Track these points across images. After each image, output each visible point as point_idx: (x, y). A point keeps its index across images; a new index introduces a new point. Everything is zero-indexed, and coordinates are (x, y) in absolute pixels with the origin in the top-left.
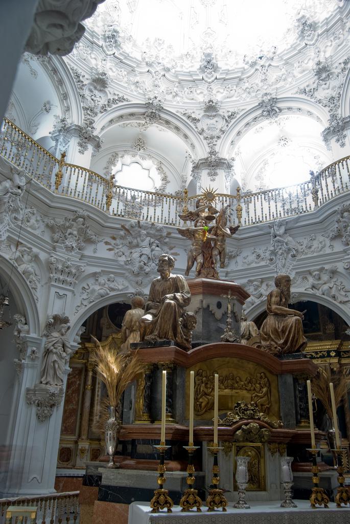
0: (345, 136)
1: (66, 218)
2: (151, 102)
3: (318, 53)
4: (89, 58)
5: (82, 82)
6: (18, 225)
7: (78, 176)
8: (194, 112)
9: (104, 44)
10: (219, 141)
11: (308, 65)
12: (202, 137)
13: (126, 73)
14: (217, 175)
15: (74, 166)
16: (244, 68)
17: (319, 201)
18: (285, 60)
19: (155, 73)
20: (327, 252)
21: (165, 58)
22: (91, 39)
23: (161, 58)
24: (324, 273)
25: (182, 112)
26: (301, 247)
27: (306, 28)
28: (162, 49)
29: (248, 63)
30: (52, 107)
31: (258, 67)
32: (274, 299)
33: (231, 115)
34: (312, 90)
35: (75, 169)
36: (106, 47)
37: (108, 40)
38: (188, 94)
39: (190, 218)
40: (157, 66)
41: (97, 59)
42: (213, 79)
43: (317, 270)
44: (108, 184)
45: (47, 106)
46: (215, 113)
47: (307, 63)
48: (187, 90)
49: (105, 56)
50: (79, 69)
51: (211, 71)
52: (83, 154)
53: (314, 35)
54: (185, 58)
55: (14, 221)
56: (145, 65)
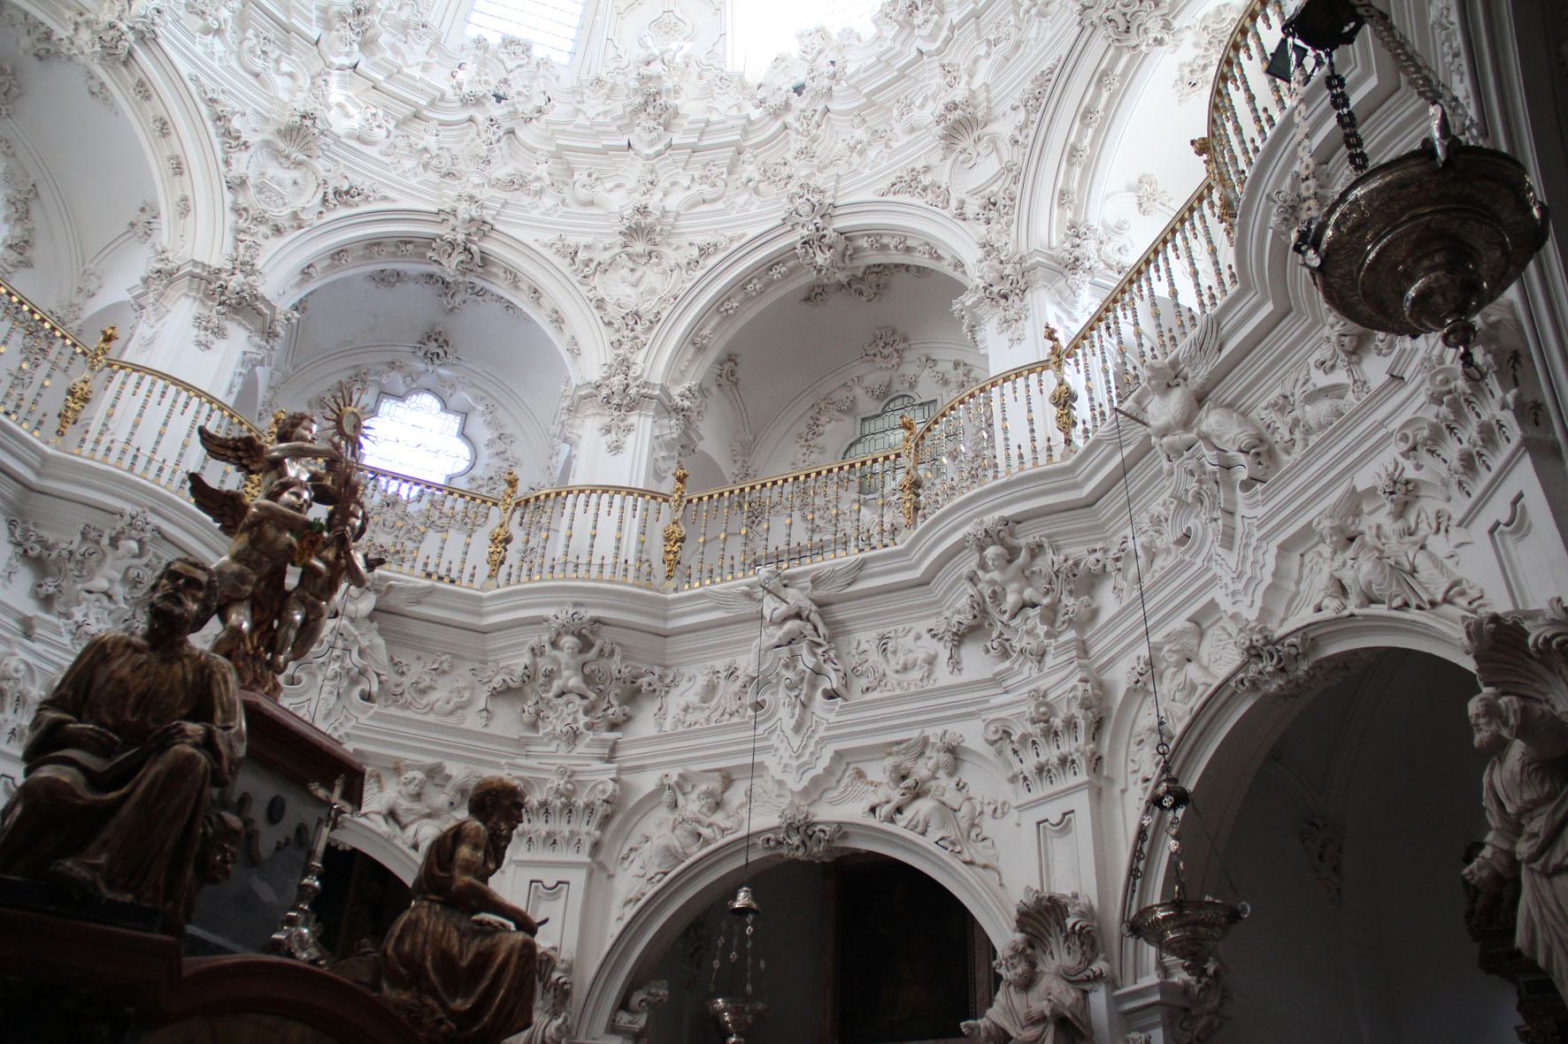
0: (629, 429)
3: (649, 186)
8: (243, 115)
10: (276, 243)
11: (611, 196)
12: (229, 197)
14: (224, 336)
16: (748, 117)
18: (558, 146)
20: (466, 725)
24: (437, 785)
26: (397, 679)
27: (650, 109)
29: (460, 86)
32: (464, 851)
33: (347, 193)
34: (593, 265)
38: (252, 51)
39: (240, 458)
42: (346, 62)
43: (420, 768)
46: (302, 157)
48: (255, 41)
51: (354, 37)
53: (659, 138)
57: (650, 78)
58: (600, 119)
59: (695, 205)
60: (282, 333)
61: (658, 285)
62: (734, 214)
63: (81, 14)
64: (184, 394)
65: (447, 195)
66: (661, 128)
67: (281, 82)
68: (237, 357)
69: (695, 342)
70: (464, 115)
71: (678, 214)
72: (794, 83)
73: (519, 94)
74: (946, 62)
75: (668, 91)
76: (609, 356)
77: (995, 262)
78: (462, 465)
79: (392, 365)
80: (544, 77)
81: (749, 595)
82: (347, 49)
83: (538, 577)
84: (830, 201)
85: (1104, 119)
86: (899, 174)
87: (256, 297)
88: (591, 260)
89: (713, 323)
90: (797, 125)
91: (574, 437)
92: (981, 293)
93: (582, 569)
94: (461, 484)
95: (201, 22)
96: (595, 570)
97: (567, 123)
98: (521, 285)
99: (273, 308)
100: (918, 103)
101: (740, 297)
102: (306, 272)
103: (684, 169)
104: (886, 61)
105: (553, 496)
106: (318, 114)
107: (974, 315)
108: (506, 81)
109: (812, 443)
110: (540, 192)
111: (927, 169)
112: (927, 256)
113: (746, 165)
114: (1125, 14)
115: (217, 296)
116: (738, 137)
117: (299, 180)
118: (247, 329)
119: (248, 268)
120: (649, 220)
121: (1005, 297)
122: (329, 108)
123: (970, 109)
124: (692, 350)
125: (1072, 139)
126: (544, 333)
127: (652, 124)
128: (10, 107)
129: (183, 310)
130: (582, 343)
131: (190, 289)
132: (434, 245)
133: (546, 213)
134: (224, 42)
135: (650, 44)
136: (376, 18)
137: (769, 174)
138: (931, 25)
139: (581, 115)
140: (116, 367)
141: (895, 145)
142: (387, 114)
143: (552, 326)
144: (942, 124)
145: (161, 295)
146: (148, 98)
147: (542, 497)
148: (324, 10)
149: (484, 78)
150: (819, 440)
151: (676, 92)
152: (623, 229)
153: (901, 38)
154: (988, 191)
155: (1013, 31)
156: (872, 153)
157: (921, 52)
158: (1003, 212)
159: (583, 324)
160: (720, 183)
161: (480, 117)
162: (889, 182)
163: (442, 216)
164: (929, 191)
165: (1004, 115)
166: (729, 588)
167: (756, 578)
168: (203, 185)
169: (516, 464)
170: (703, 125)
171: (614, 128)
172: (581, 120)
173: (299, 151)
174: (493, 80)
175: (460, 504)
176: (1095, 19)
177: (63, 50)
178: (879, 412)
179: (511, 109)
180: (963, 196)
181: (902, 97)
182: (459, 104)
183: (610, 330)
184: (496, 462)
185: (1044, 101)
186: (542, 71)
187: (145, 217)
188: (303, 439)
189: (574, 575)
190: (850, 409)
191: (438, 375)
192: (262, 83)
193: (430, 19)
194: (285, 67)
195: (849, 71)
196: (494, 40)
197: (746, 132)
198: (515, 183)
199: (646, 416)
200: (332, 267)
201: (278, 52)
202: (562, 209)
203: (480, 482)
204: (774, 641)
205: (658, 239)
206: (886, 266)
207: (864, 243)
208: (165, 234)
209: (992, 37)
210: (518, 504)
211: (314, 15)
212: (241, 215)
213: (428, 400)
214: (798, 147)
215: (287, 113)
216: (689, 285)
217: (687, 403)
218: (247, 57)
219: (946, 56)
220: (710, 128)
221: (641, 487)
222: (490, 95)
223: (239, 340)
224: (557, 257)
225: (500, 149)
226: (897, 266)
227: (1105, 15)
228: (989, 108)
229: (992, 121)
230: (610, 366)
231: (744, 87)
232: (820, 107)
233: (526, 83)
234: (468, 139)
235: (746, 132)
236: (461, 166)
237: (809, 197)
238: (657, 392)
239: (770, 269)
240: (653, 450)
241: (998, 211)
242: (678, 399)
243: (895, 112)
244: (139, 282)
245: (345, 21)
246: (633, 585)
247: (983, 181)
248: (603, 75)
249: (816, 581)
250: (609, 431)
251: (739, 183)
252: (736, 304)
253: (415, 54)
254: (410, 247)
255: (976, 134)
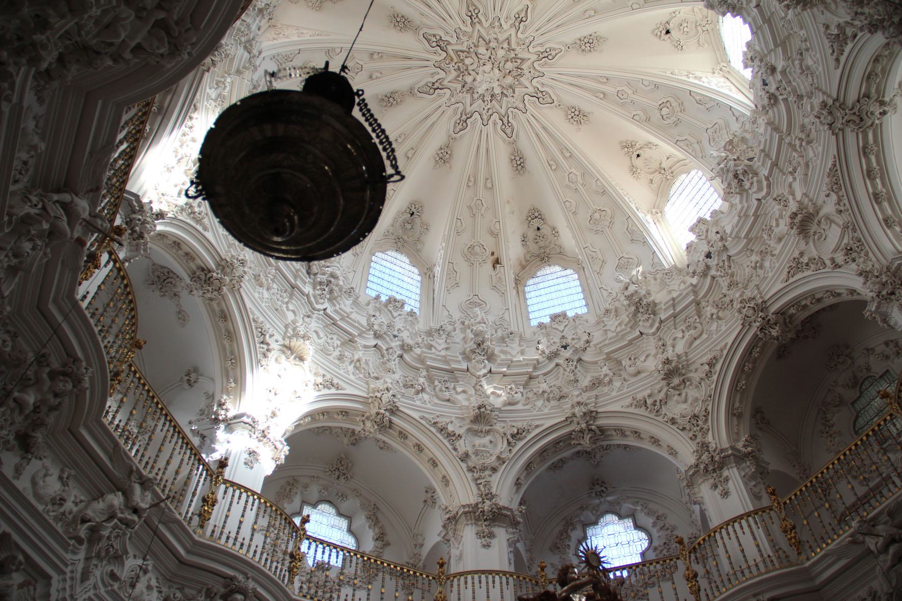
0: (727, 480)
1: (208, 590)
2: (379, 395)
3: (663, 348)
4: (285, 309)
5: (268, 344)
6: (113, 590)
7: (245, 508)
8: (452, 422)
9: (311, 292)
12: (464, 465)
13: (339, 343)
15: (240, 487)
16: (692, 285)
17: (702, 593)
19: (387, 350)
21: (402, 329)
22: (293, 281)
23: (396, 328)
25: (431, 420)
27: (641, 310)
28: (400, 315)
29: (543, 352)
30: (201, 379)
31: (560, 361)
33: (518, 433)
34: (658, 403)
35: (241, 493)
36: (315, 297)
37: (318, 287)
38: (441, 390)
40: (391, 340)
41: (297, 313)
42: (485, 371)
44: (296, 532)
45: (193, 376)
46: (488, 428)
47: (645, 361)
48: (440, 385)
49: (310, 311)
50: (266, 322)
51: (483, 358)
52: (252, 468)
53: (654, 321)
54: (436, 335)
55: (107, 579)
56: (372, 336)
57: (632, 295)
58: (619, 329)
59: (691, 344)
60: (521, 520)
61: (697, 395)
62: (715, 337)
63: (363, 416)
64: (490, 577)
65: (566, 408)
66: (652, 316)
67: (460, 397)
68: (505, 544)
69: (733, 414)
70: (552, 365)
71: (686, 353)
72: (703, 254)
73: (573, 339)
74: (775, 196)
75: (645, 295)
76: (693, 446)
77: (873, 279)
78: (645, 544)
79: (582, 508)
80: (580, 324)
81: (854, 542)
82: (483, 365)
83: (724, 590)
84: (760, 301)
85: (881, 169)
86: (788, 265)
87: (500, 509)
88: (655, 401)
89: (738, 399)
90: (719, 273)
91: (699, 499)
92: (877, 300)
93: (746, 572)
94: (651, 556)
95: (413, 390)
96: (754, 569)
97: (605, 340)
98: (627, 433)
99: (511, 510)
100: (774, 225)
101: (744, 376)
102: (518, 484)
103: (675, 329)
104: (744, 215)
105: (707, 538)
106: (485, 403)
107: (881, 314)
108: (563, 337)
109: (831, 432)
110: (610, 381)
111: (802, 254)
112: (831, 297)
113: (706, 309)
114: (854, 114)
115: (481, 517)
116: (693, 297)
117: (492, 440)
118: (503, 527)
119: (490, 496)
120: (673, 365)
121: (893, 293)
122: (488, 397)
123: (805, 211)
124: (735, 419)
125: (871, 190)
126: (660, 455)
127: (646, 316)
128: (351, 474)
129: (469, 533)
130: (675, 448)
131: (467, 520)
132: (573, 437)
133: (620, 389)
134: (427, 393)
135: (622, 278)
136: (488, 343)
137: (720, 306)
138: (755, 184)
139: (608, 332)
140: (451, 578)
141: (776, 252)
142: (516, 385)
143: (653, 446)
144: (795, 227)
145: (455, 530)
146: (406, 438)
147: (702, 542)
148: (464, 353)
149: (552, 341)
150: (834, 428)
151: (649, 294)
152: (662, 376)
153: (744, 200)
154: (843, 245)
155: (800, 159)
156: (767, 264)
157: (758, 200)
158: (858, 250)
159: (669, 436)
160: (698, 325)
161: (560, 361)
162: (785, 273)
163: (569, 420)
164: (811, 265)
165: (824, 202)
166: (839, 543)
167: (852, 530)
168: (450, 467)
169: (674, 528)
170: (672, 302)
171: (629, 329)
172: (610, 335)
173: (485, 425)
174: (557, 340)
175: (659, 567)
176: (839, 126)
177: (362, 436)
178: (858, 394)
179: (574, 349)
180: (831, 256)
181: (764, 227)
182: (547, 361)
183: (686, 432)
184: (662, 533)
185: (841, 182)
186: (577, 322)
187: (429, 495)
188: (574, 579)
189: (744, 579)
190: (841, 402)
191: (609, 502)
192: (453, 403)
193: (513, 328)
194: (459, 389)
195: (728, 231)
196: (547, 320)
197: (695, 293)
198: (596, 383)
199: (732, 467)
200: (528, 475)
201: (453, 384)
202: (626, 384)
203: (661, 548)
204: (889, 564)
205: (683, 371)
206: (811, 316)
207: (792, 311)
208: (443, 498)
209: (791, 170)
210: (690, 553)
211: (460, 358)
212: (473, 472)
213: (609, 517)
214: (727, 285)
215: (471, 410)
216: (713, 386)
217: (749, 449)
218: (440, 394)
219: (774, 192)
220: (676, 301)
221: (752, 509)
222: (560, 348)
223: (502, 535)
224: (637, 409)
225: (579, 371)
226: (817, 312)
227: (844, 121)
228: (814, 204)
229: (820, 209)
230: (697, 451)
231: (680, 271)
232: (725, 258)
233: (573, 332)
234: (561, 375)
235: (695, 293)
236: (565, 390)
237: (748, 305)
238: (730, 452)
239: (751, 353)
240: (746, 484)
241: (856, 251)
242: (743, 449)
243: (766, 237)
244: (441, 528)
245: (475, 352)
246: (781, 568)
247: (837, 240)
248: (608, 307)
249: (891, 514)
250: (716, 487)
251: (708, 320)
252: (744, 382)
253: (514, 347)
254: (561, 444)
255: (816, 221)
